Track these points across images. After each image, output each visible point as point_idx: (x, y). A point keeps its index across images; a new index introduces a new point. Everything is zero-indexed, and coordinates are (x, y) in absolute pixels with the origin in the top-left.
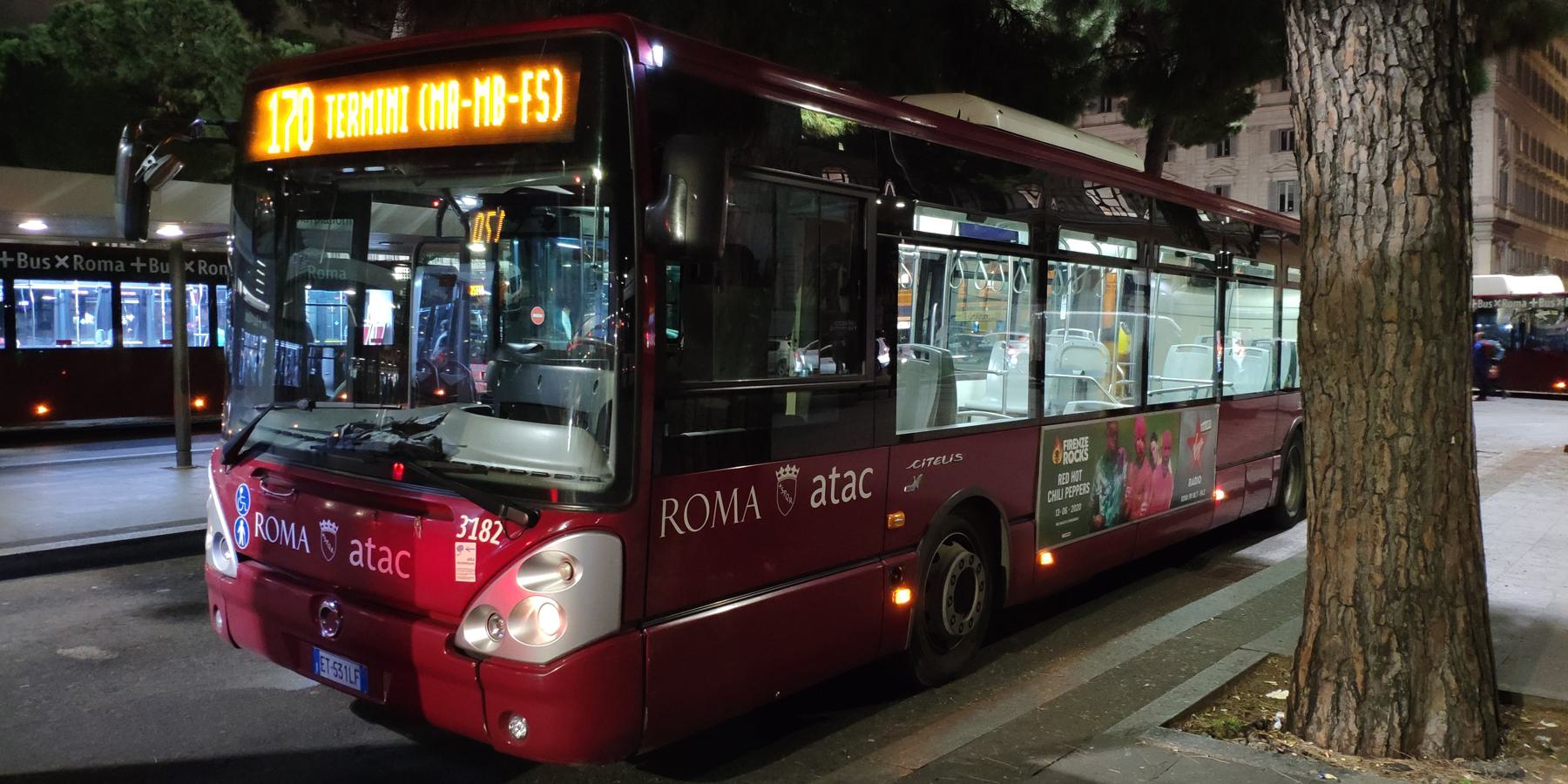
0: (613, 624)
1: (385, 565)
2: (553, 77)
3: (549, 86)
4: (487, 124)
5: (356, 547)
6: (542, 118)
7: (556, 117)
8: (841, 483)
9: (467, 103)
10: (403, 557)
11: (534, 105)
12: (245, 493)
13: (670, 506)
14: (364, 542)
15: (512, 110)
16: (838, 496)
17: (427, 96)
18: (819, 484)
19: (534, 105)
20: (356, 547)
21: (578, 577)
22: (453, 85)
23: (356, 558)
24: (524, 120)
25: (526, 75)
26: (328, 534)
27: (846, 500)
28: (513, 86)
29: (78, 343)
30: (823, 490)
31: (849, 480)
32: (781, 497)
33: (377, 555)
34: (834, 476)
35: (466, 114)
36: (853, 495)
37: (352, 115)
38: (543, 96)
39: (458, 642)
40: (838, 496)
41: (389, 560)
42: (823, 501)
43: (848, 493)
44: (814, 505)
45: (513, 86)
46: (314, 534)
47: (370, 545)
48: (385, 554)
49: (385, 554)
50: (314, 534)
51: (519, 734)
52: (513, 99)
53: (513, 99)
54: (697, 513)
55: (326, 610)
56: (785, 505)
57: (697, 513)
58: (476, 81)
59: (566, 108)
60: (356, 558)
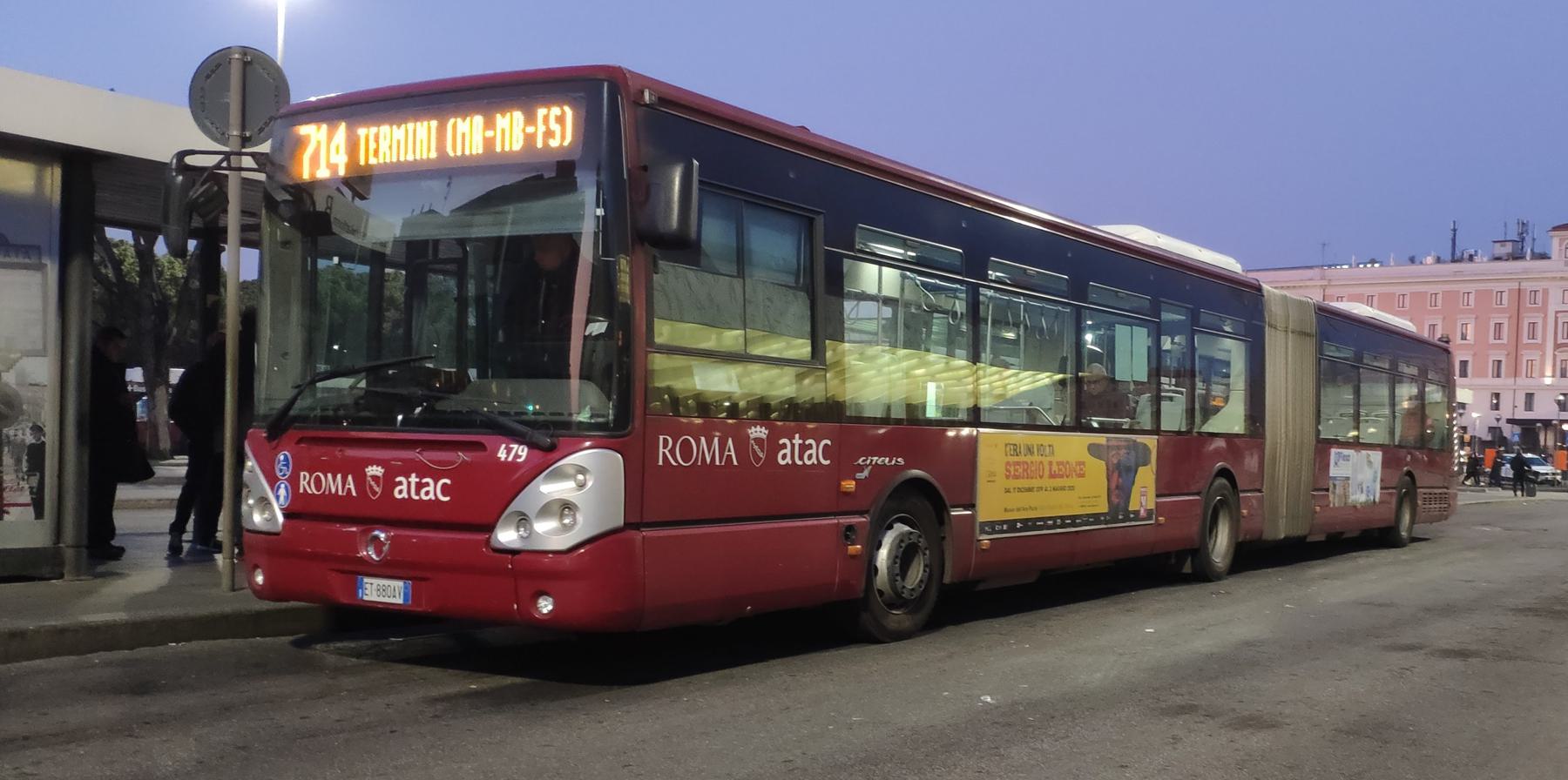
0: (620, 522)
1: (427, 493)
2: (563, 113)
3: (561, 120)
4: (507, 149)
5: (400, 483)
6: (554, 143)
7: (566, 143)
8: (804, 448)
9: (490, 134)
10: (444, 485)
11: (549, 134)
12: (286, 459)
13: (666, 441)
14: (407, 476)
15: (529, 139)
16: (801, 458)
17: (455, 127)
18: (784, 446)
19: (549, 134)
20: (400, 483)
21: (590, 484)
22: (478, 120)
23: (400, 493)
24: (540, 145)
25: (541, 112)
26: (375, 478)
27: (808, 463)
28: (530, 119)
29: (56, 197)
30: (788, 451)
31: (810, 446)
32: (754, 452)
33: (420, 486)
34: (797, 441)
35: (489, 143)
36: (814, 460)
37: (384, 147)
38: (555, 127)
39: (494, 543)
40: (801, 458)
41: (431, 489)
42: (788, 460)
43: (810, 457)
44: (782, 462)
45: (530, 119)
46: (360, 480)
47: (414, 479)
48: (427, 484)
49: (427, 484)
50: (360, 480)
51: (545, 611)
52: (530, 130)
53: (530, 130)
54: (686, 451)
55: (377, 538)
56: (758, 459)
57: (686, 451)
58: (498, 116)
59: (573, 136)
60: (400, 493)
